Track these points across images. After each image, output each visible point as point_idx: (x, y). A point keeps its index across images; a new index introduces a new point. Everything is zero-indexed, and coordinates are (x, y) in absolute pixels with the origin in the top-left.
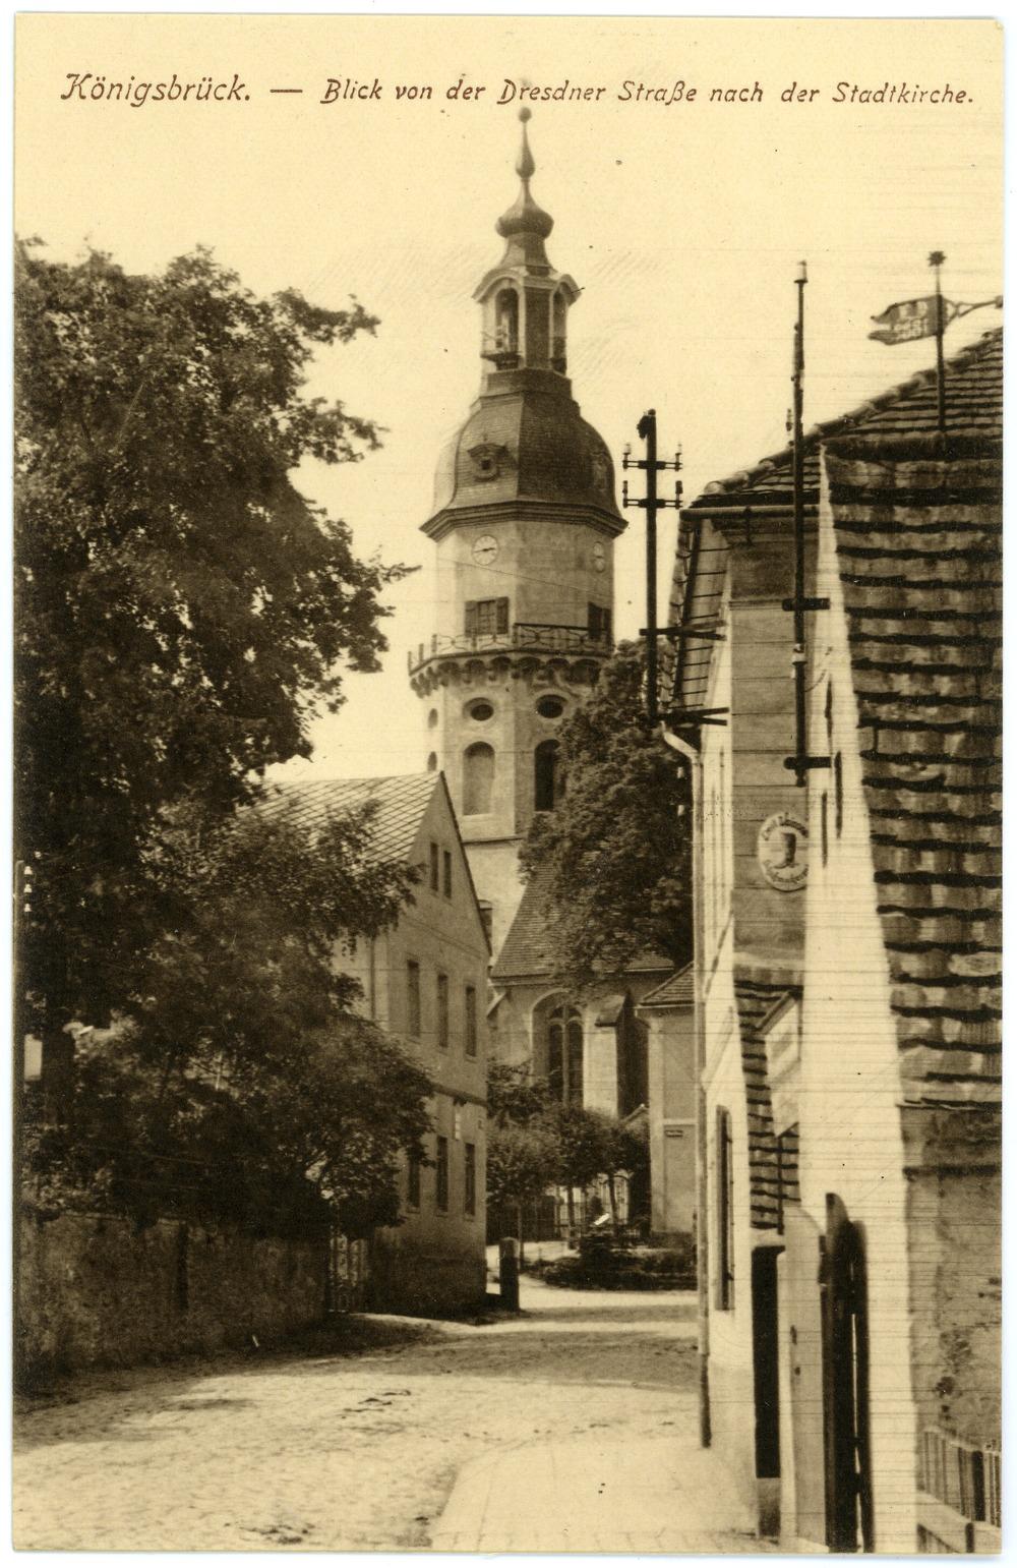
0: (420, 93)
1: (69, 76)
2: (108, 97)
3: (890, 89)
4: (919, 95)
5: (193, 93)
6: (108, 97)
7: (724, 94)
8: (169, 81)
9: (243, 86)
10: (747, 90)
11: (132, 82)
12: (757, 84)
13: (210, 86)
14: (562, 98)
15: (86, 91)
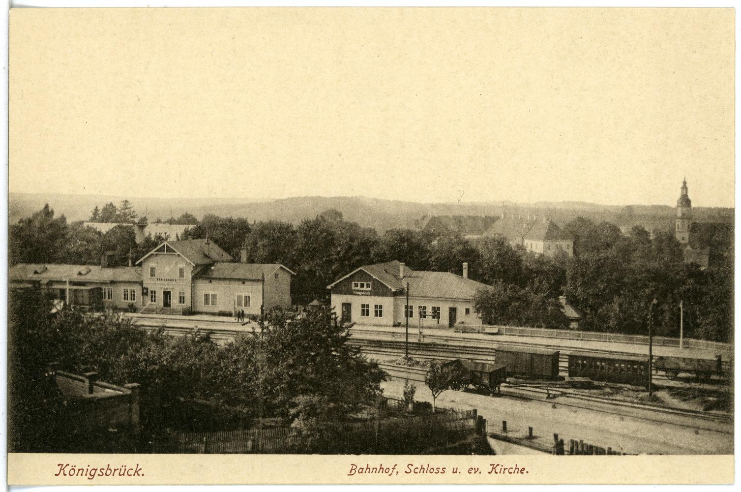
0: (76, 472)
1: (59, 465)
4: (503, 470)
5: (118, 472)
7: (384, 470)
8: (106, 468)
9: (141, 469)
11: (88, 468)
12: (381, 465)
13: (125, 469)
14: (362, 472)
15: (67, 472)
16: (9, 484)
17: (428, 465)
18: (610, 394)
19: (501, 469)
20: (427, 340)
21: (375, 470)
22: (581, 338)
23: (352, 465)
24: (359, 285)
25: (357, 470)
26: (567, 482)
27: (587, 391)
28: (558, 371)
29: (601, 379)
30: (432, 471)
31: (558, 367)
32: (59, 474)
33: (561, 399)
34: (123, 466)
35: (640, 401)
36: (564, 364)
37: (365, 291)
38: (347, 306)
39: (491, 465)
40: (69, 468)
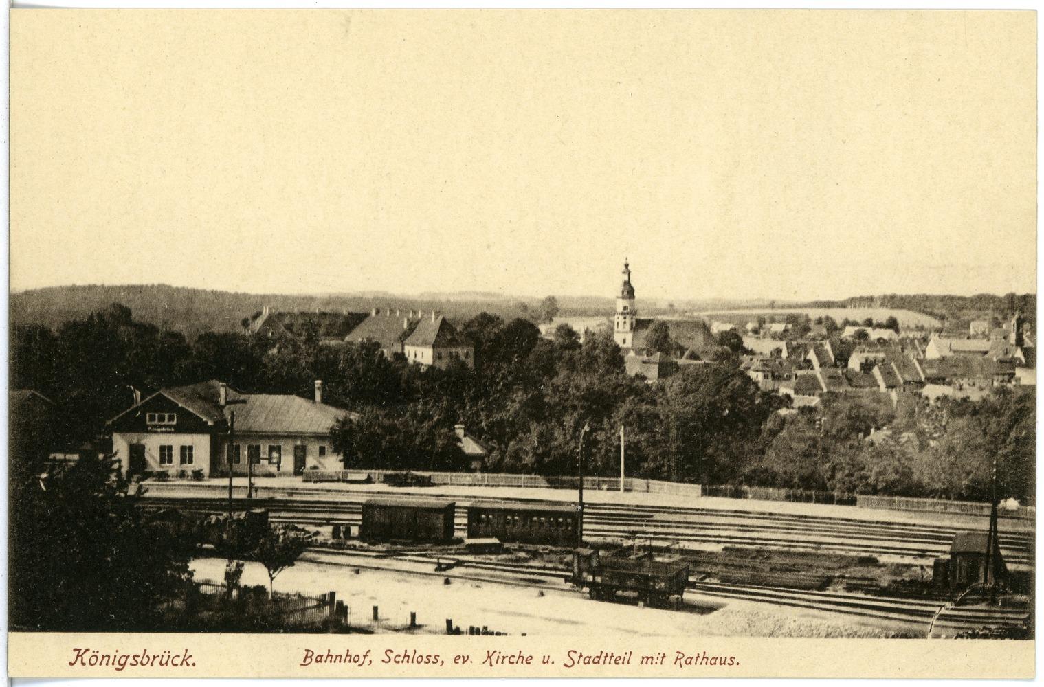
2: (100, 664)
3: (604, 655)
5: (157, 661)
6: (100, 664)
7: (525, 659)
8: (141, 654)
9: (191, 656)
10: (514, 656)
12: (406, 651)
13: (169, 656)
16: (10, 675)
17: (415, 651)
18: (526, 560)
19: (498, 657)
20: (262, 495)
21: (339, 658)
22: (486, 483)
23: (678, 652)
24: (166, 417)
25: (314, 658)
26: (425, 676)
27: (493, 557)
28: (453, 530)
29: (512, 540)
30: (420, 659)
31: (454, 524)
32: (75, 663)
33: (456, 571)
34: (165, 652)
35: (565, 568)
36: (461, 520)
37: (166, 426)
38: (137, 452)
39: (75, 650)
40: (496, 654)
